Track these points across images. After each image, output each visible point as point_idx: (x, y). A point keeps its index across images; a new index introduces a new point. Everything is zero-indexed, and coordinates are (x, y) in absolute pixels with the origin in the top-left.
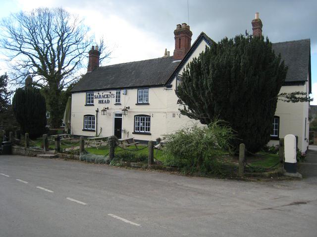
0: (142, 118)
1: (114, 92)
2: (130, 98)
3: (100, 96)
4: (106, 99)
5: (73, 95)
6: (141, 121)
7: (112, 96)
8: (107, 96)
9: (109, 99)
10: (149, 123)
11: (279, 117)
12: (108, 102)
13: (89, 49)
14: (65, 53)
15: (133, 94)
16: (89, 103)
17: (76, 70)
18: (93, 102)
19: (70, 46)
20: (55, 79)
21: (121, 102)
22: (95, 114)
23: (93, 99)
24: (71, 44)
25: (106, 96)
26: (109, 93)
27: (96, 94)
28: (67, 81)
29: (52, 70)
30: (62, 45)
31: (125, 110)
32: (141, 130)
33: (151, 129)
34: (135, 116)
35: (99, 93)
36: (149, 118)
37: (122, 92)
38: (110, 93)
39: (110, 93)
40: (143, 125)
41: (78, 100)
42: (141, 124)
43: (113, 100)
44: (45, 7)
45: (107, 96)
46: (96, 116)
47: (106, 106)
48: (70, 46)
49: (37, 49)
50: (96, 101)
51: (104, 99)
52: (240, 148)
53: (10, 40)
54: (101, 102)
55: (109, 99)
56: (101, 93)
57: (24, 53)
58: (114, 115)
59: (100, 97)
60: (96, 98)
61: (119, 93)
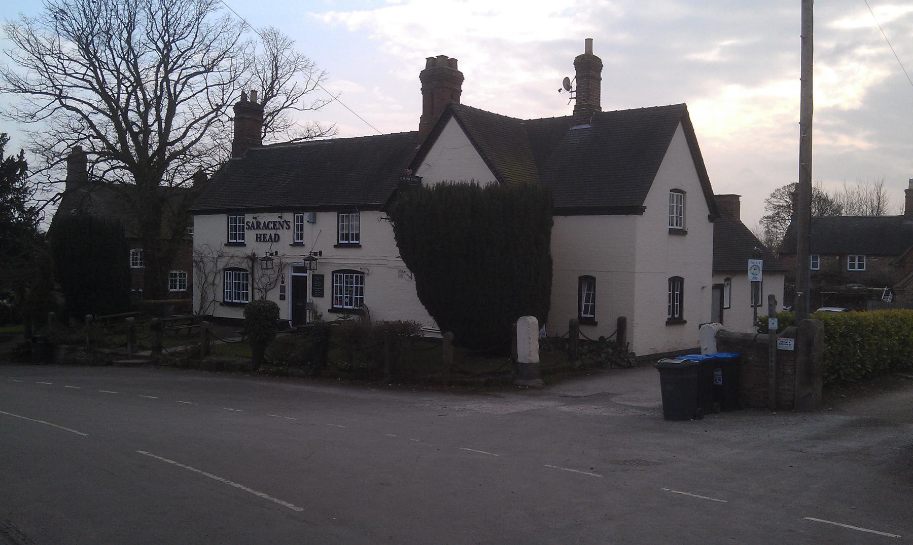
1: (289, 217)
2: (322, 231)
3: (258, 223)
4: (273, 232)
5: (717, 191)
7: (285, 226)
8: (275, 225)
9: (279, 232)
12: (277, 239)
13: (236, 96)
14: (176, 97)
15: (328, 222)
16: (235, 239)
17: (202, 136)
20: (149, 167)
21: (304, 241)
23: (243, 230)
24: (192, 71)
25: (271, 225)
27: (249, 218)
28: (179, 175)
29: (142, 147)
30: (166, 79)
31: (310, 259)
34: (334, 272)
36: (362, 278)
37: (306, 216)
41: (209, 232)
43: (287, 236)
45: (275, 225)
46: (250, 271)
49: (102, 90)
50: (250, 236)
51: (268, 232)
53: (98, 119)
54: (260, 238)
55: (279, 232)
56: (265, 218)
59: (258, 227)
60: (249, 228)
61: (302, 217)
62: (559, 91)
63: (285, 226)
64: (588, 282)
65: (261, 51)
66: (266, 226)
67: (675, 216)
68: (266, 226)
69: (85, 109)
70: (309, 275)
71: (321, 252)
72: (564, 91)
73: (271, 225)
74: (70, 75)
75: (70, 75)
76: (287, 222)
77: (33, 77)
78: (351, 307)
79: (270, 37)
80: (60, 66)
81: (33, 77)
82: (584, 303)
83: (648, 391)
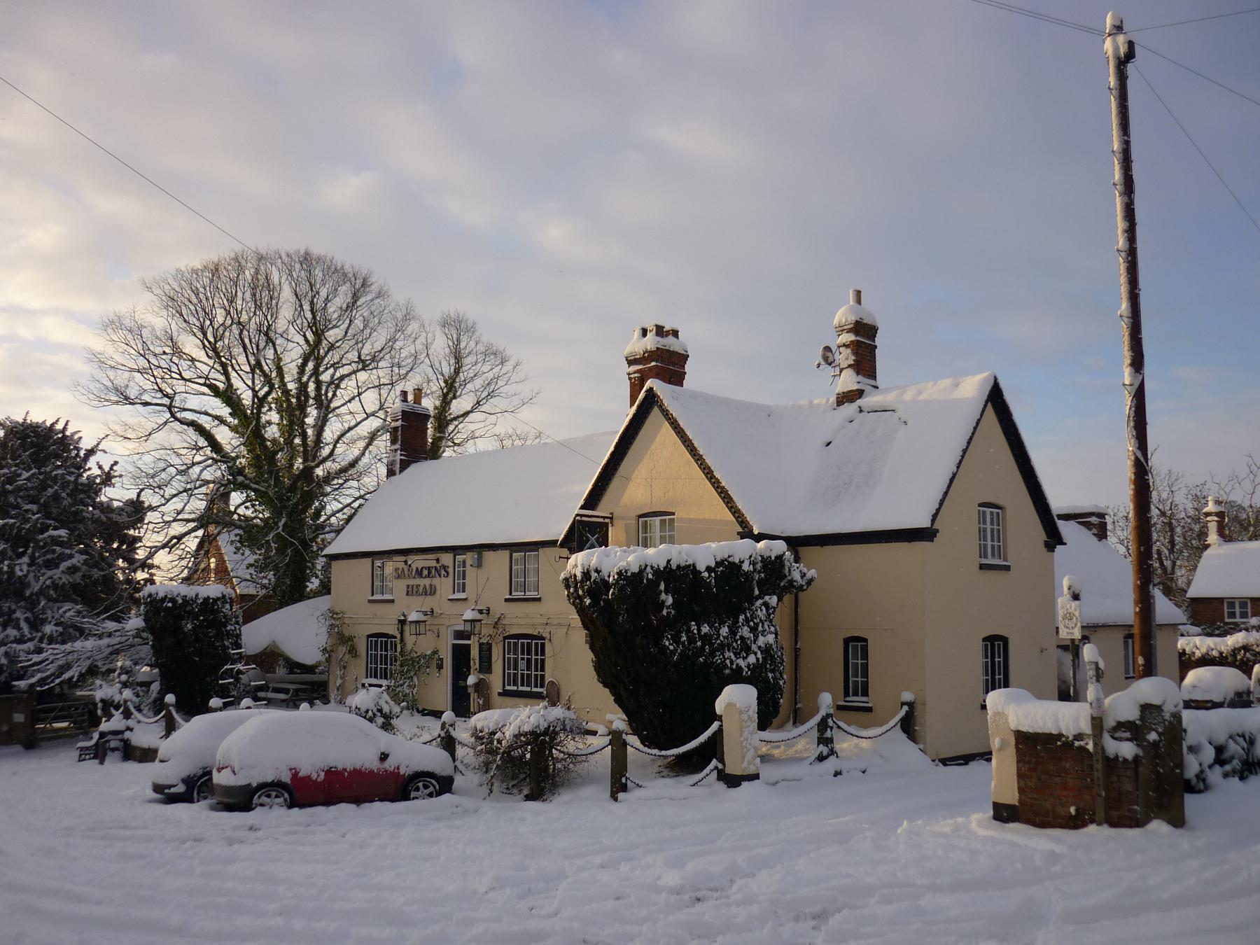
0: (523, 644)
4: (427, 582)
6: (523, 653)
8: (429, 573)
10: (543, 661)
11: (866, 640)
18: (865, 694)
19: (342, 378)
22: (392, 630)
25: (425, 572)
26: (433, 563)
32: (523, 685)
33: (1009, 556)
34: (369, 636)
35: (406, 562)
36: (543, 645)
38: (438, 561)
39: (438, 561)
40: (529, 668)
42: (522, 665)
44: (330, 255)
45: (429, 573)
46: (399, 636)
47: (428, 603)
48: (342, 378)
49: (228, 396)
52: (576, 616)
57: (177, 419)
58: (450, 636)
62: (819, 365)
63: (443, 572)
64: (856, 646)
65: (441, 345)
66: (419, 573)
67: (989, 543)
68: (419, 573)
69: (204, 421)
70: (474, 643)
71: (488, 610)
72: (824, 365)
73: (425, 572)
74: (189, 380)
75: (189, 380)
76: (445, 568)
77: (140, 384)
78: (528, 689)
79: (457, 327)
80: (174, 369)
81: (140, 384)
82: (851, 679)
83: (1001, 777)
